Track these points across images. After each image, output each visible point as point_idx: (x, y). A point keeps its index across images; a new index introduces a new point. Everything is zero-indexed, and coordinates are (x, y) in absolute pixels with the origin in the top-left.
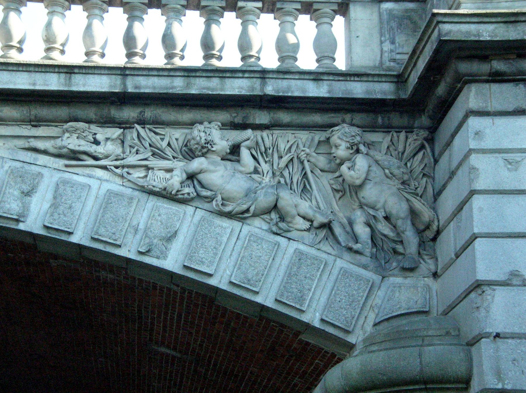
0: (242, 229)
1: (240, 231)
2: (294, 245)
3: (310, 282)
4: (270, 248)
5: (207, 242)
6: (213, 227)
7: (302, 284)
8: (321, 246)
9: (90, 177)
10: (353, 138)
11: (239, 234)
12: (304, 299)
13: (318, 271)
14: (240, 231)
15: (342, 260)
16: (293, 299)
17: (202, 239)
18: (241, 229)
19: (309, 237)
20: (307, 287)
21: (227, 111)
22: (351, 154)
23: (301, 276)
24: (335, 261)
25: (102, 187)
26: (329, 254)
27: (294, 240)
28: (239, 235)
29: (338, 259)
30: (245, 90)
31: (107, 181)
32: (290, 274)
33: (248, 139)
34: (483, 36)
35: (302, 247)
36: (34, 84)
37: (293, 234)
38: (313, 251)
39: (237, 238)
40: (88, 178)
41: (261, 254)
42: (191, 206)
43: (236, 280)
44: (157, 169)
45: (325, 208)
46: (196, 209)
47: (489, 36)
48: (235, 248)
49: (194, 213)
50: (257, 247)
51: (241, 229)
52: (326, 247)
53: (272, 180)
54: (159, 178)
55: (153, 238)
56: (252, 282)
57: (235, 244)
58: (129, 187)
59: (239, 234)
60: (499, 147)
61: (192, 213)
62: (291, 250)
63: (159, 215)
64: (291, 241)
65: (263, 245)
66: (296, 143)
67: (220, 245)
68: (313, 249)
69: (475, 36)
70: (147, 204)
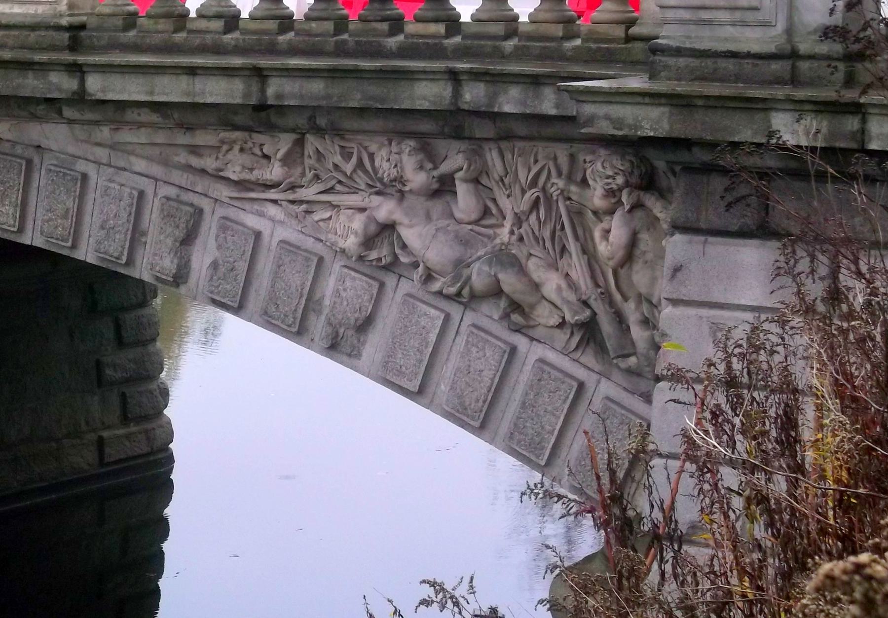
0: (464, 318)
1: (461, 321)
2: (539, 351)
3: (553, 419)
4: (497, 357)
5: (407, 340)
6: (416, 316)
7: (541, 423)
8: (577, 355)
9: (260, 216)
10: (609, 181)
11: (460, 324)
12: (543, 448)
13: (565, 401)
14: (461, 321)
15: (609, 383)
16: (526, 446)
17: (401, 335)
18: (462, 317)
19: (562, 337)
20: (548, 427)
21: (186, 333)
22: (615, 203)
23: (540, 408)
24: (599, 382)
25: (275, 234)
26: (589, 369)
27: (539, 341)
28: (459, 327)
29: (603, 380)
30: (429, 101)
31: (282, 223)
32: (524, 403)
33: (461, 169)
34: (642, 127)
35: (552, 356)
36: (151, 93)
37: (538, 333)
38: (565, 363)
39: (457, 332)
40: (258, 218)
41: (482, 367)
42: (394, 272)
43: (448, 406)
44: (344, 207)
45: (587, 288)
46: (399, 278)
47: (651, 129)
48: (454, 348)
49: (397, 285)
50: (477, 355)
51: (462, 317)
52: (589, 358)
53: (515, 229)
54: (342, 225)
55: (338, 326)
56: (469, 412)
57: (454, 341)
58: (310, 236)
59: (460, 324)
60: (706, 300)
61: (394, 284)
62: (532, 359)
63: (345, 290)
64: (534, 342)
65: (487, 351)
66: (547, 167)
67: (426, 347)
68: (567, 358)
69: (630, 127)
70: (334, 265)
